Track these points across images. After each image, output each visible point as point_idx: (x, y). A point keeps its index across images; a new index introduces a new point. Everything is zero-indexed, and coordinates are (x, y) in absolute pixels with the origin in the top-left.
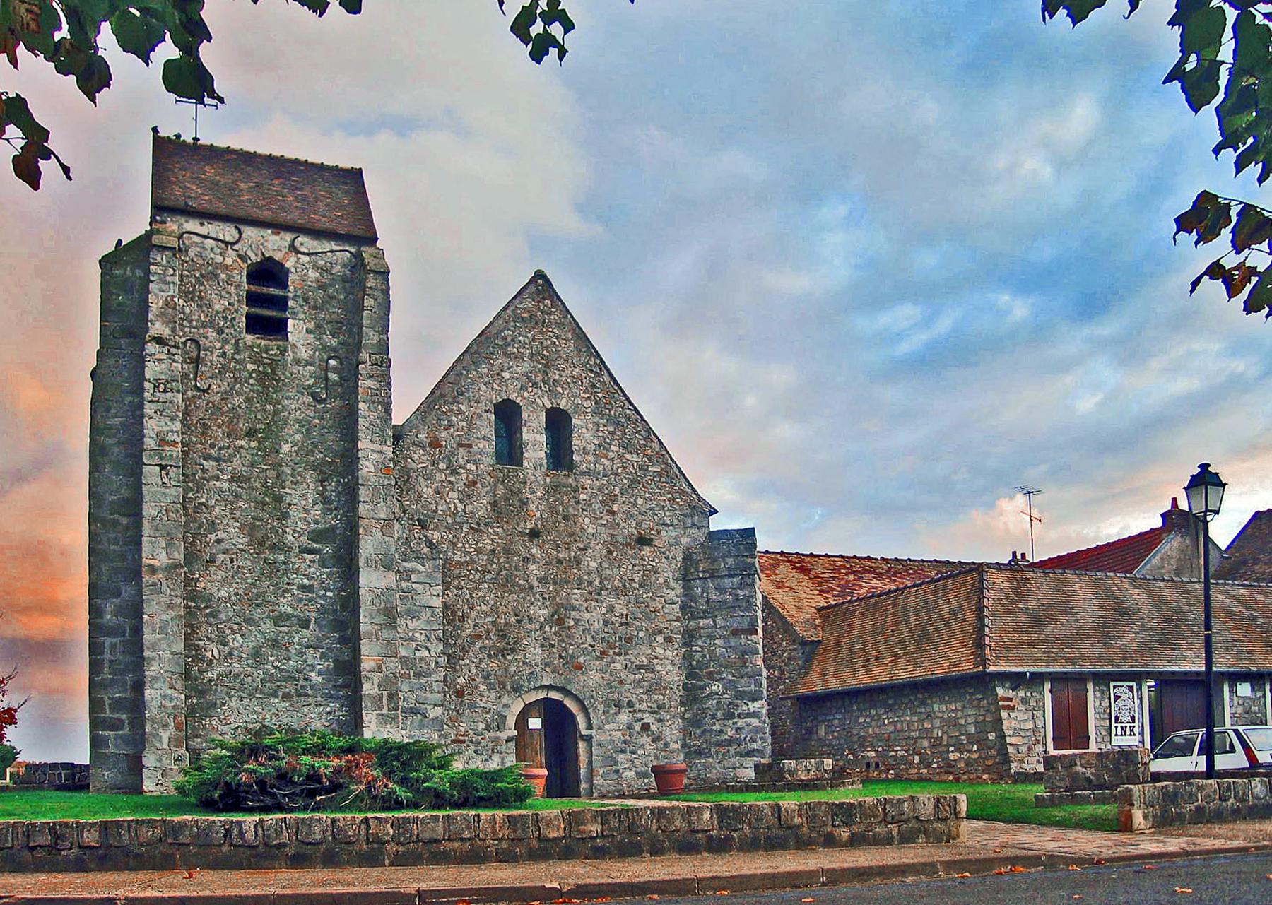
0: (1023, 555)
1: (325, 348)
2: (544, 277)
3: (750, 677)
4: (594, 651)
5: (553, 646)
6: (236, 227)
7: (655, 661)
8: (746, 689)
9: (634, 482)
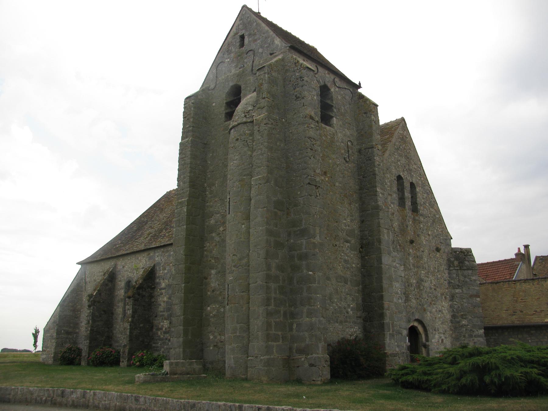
3: (478, 318)
5: (418, 299)
6: (316, 66)
8: (477, 323)
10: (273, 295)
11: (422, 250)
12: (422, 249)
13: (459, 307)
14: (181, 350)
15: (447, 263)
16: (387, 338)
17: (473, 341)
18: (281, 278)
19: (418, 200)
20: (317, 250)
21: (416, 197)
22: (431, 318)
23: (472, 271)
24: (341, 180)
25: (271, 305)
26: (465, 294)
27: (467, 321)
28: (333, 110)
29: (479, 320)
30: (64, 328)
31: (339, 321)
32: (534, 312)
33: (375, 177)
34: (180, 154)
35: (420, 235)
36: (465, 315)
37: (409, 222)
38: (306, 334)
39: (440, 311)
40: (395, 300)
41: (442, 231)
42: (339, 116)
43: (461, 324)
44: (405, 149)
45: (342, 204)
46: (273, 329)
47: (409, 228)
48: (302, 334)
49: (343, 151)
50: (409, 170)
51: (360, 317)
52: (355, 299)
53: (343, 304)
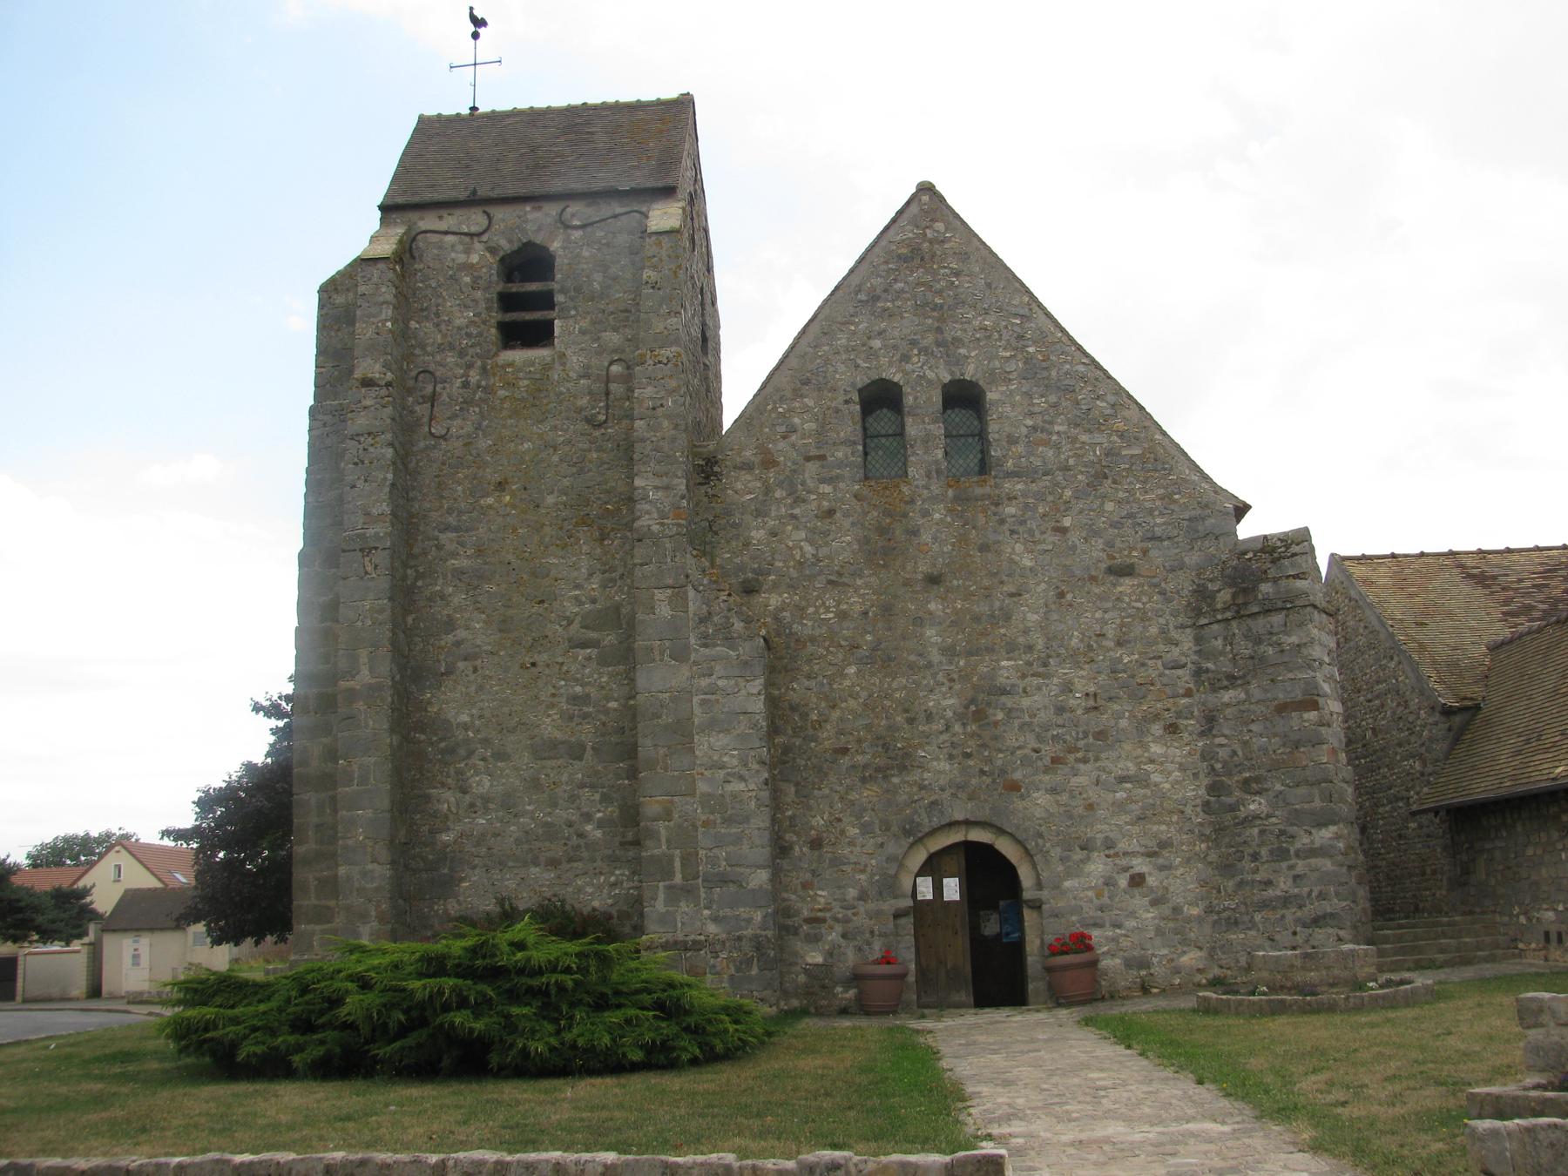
5: (968, 756)
13: (1234, 753)
15: (1189, 604)
36: (1257, 779)
43: (1242, 813)
47: (926, 537)
53: (562, 814)
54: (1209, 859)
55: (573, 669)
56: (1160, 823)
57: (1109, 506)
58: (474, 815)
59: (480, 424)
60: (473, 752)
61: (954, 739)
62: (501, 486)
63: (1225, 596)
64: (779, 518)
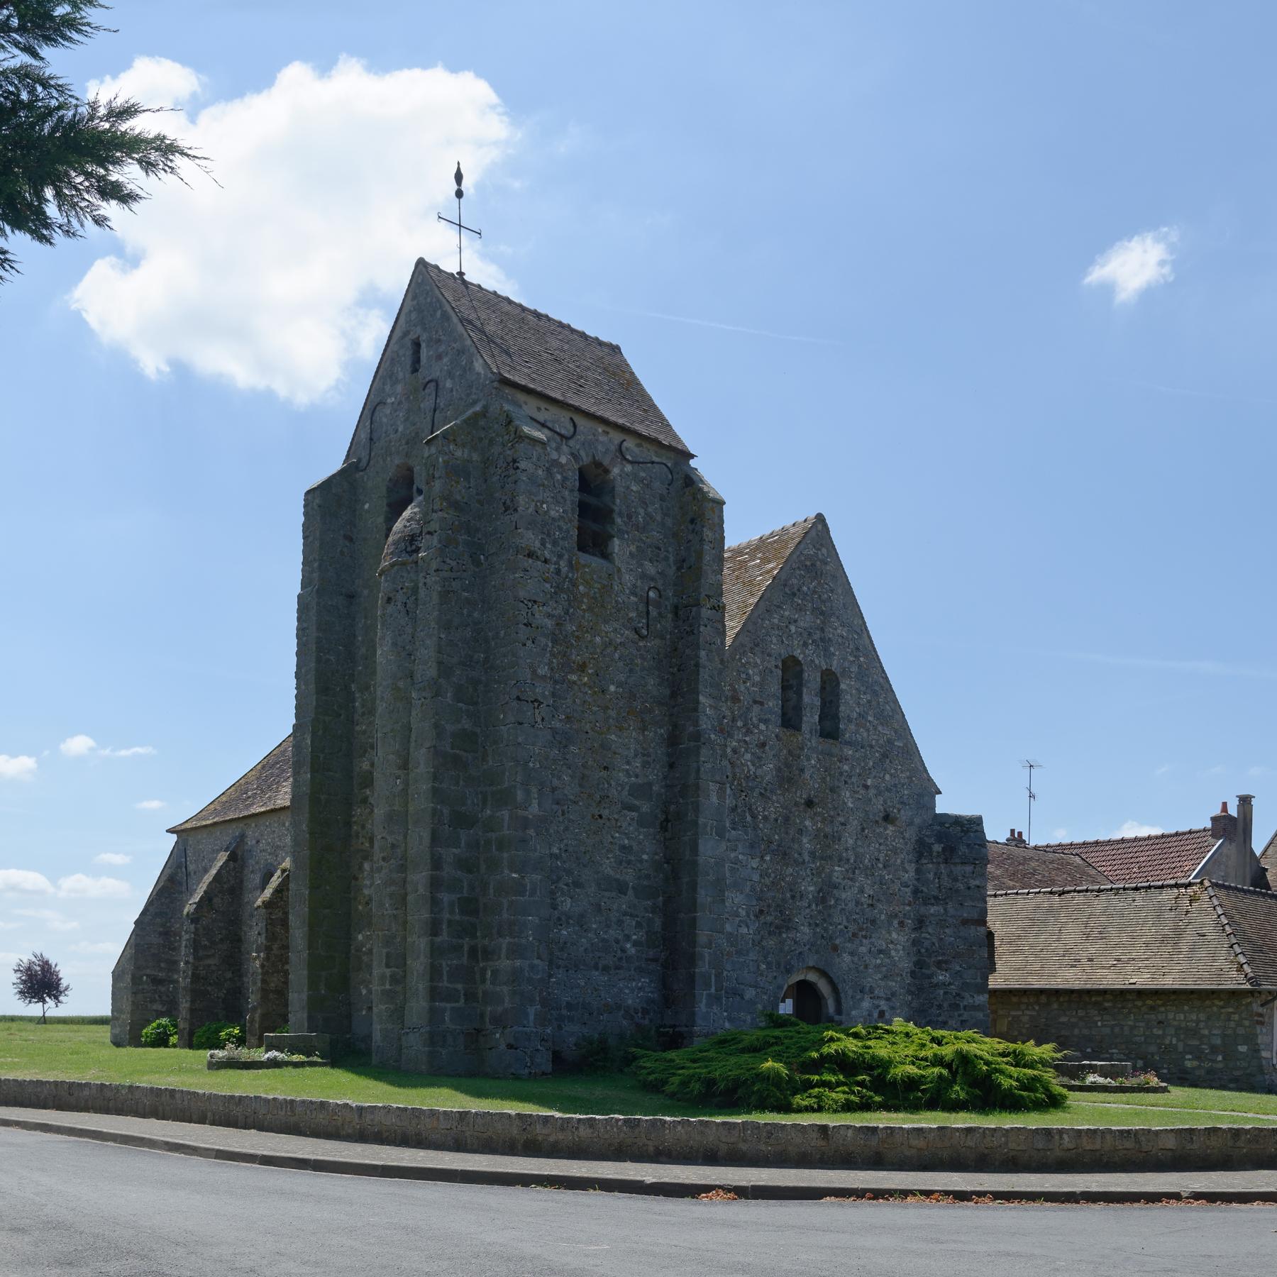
0: (1020, 834)
1: (643, 576)
2: (824, 520)
4: (847, 932)
5: (817, 925)
7: (891, 946)
9: (885, 756)
10: (446, 916)
11: (843, 820)
12: (841, 819)
13: (934, 944)
14: (305, 1015)
15: (915, 849)
16: (701, 1002)
17: (961, 1018)
18: (465, 884)
19: (842, 708)
20: (531, 832)
21: (838, 701)
22: (852, 966)
23: (975, 867)
24: (623, 679)
25: (441, 935)
26: (951, 917)
27: (950, 975)
28: (613, 519)
29: (979, 974)
30: (148, 971)
31: (600, 965)
32: (1115, 962)
33: (698, 671)
34: (299, 619)
35: (838, 787)
36: (946, 962)
37: (809, 759)
38: (505, 989)
39: (880, 952)
40: (728, 928)
41: (910, 778)
42: (628, 533)
43: (935, 980)
44: (815, 592)
45: (620, 730)
46: (445, 978)
47: (807, 775)
48: (498, 989)
49: (633, 615)
50: (822, 640)
51: (655, 960)
52: (644, 924)
53: (613, 933)
54: (912, 1005)
55: (624, 826)
56: (893, 981)
57: (887, 777)
58: (559, 927)
59: (568, 610)
60: (561, 878)
61: (812, 913)
62: (582, 668)
63: (937, 848)
64: (739, 741)
